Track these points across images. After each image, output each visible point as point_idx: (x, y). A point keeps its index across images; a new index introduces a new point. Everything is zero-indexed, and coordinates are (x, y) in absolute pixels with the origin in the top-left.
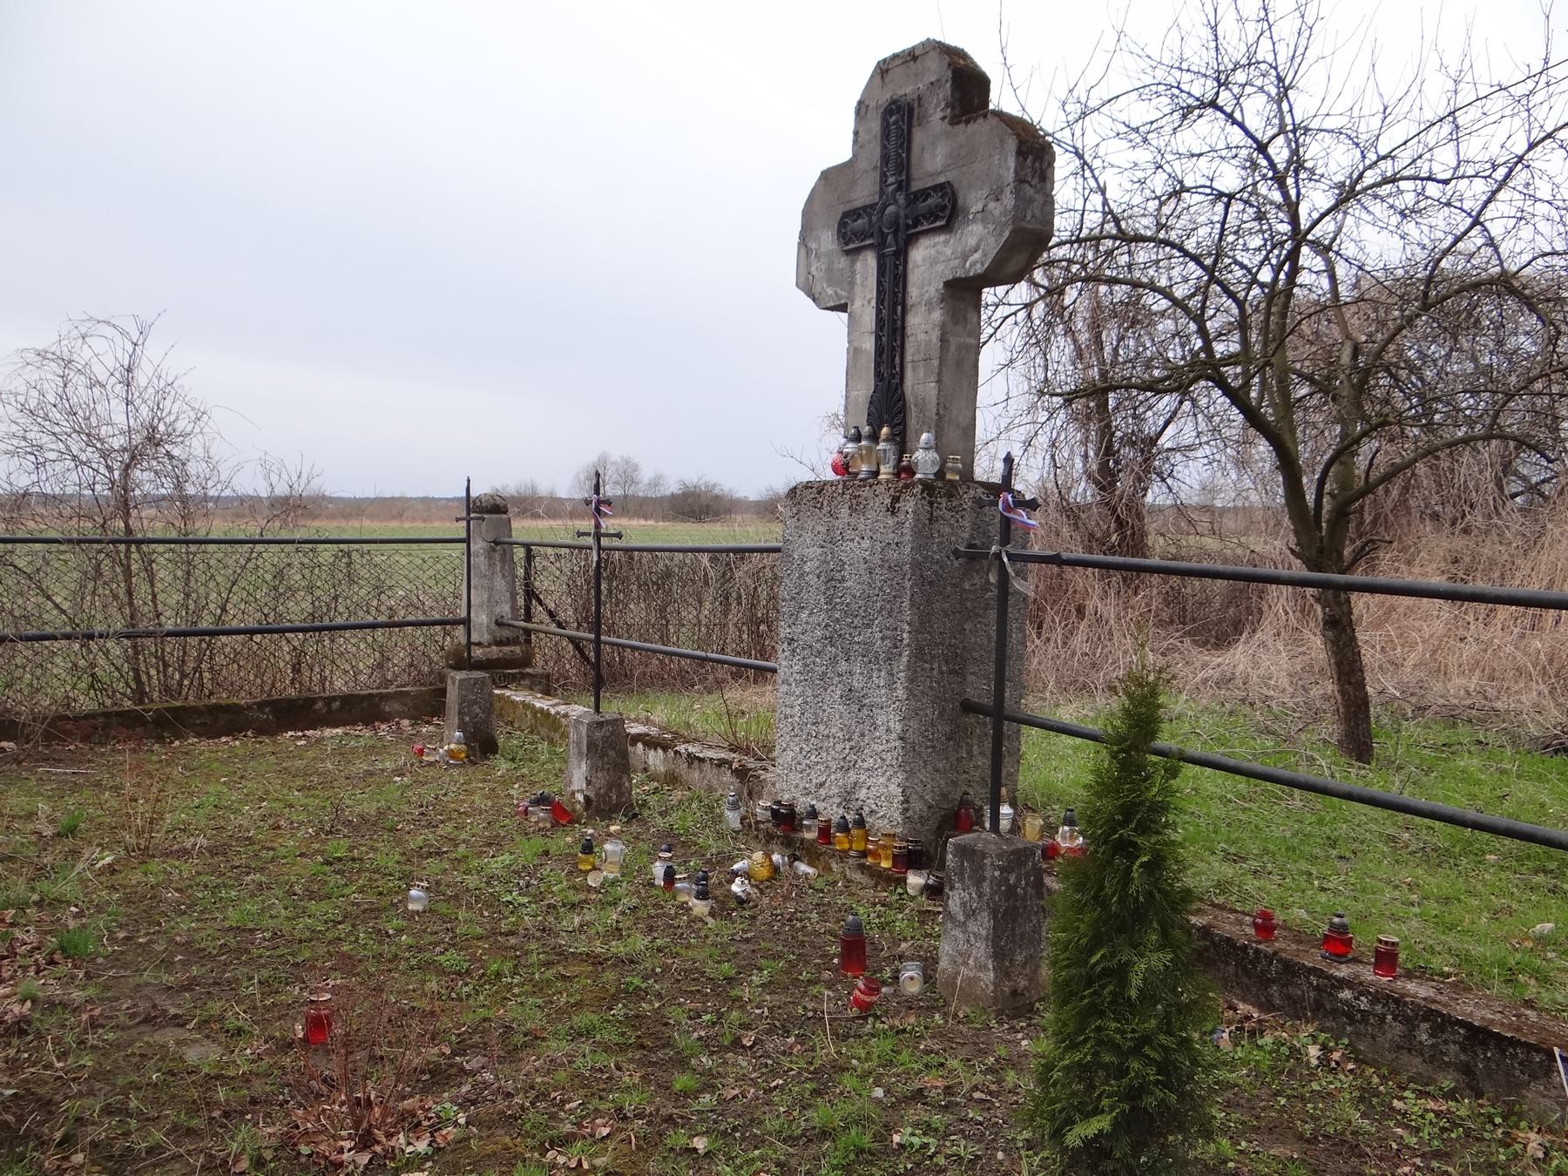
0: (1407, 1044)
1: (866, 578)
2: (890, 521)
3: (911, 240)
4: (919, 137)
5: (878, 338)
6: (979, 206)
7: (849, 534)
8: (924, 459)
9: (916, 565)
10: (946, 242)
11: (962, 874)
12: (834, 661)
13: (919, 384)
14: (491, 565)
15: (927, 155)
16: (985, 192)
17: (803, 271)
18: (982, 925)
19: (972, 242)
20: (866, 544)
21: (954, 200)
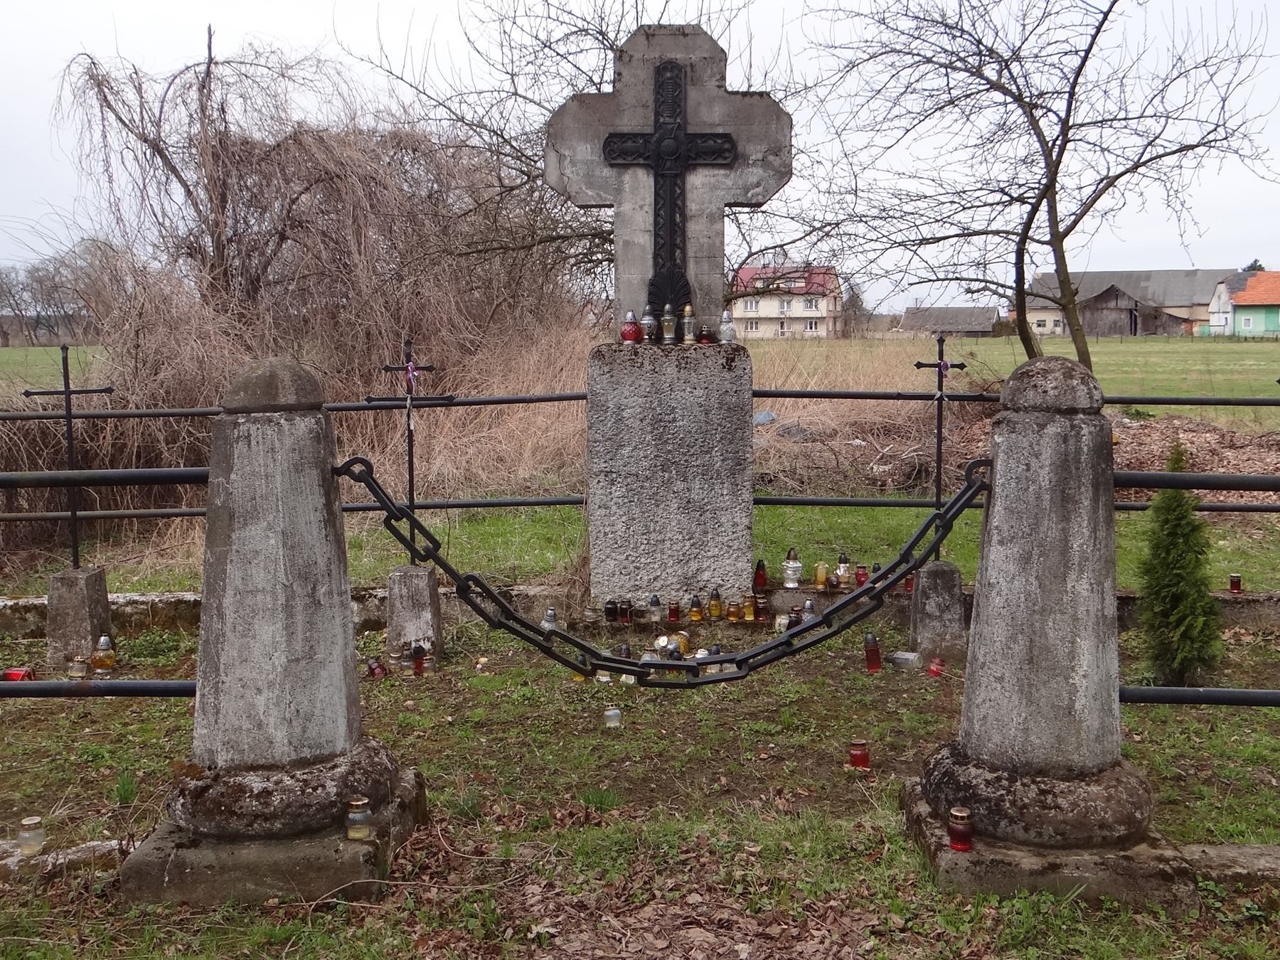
1: (703, 418)
2: (727, 375)
3: (694, 167)
6: (760, 156)
10: (727, 176)
11: (936, 588)
16: (764, 147)
19: (754, 180)
21: (734, 145)
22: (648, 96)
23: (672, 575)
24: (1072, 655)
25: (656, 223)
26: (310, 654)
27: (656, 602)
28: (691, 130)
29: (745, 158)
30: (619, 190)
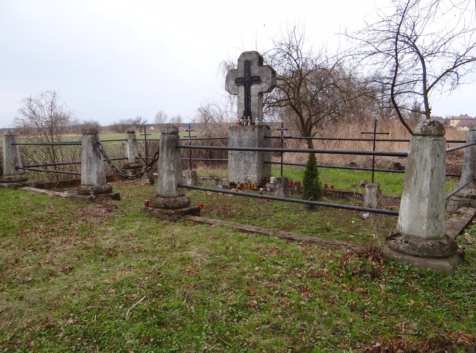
0: (336, 196)
2: (253, 132)
3: (251, 84)
4: (252, 67)
5: (245, 101)
7: (244, 135)
8: (257, 122)
9: (258, 139)
12: (242, 156)
13: (254, 109)
14: (134, 145)
15: (254, 71)
17: (246, 91)
18: (282, 188)
19: (264, 86)
20: (248, 136)
22: (243, 69)
23: (243, 177)
24: (163, 176)
25: (245, 98)
26: (90, 170)
27: (239, 183)
28: (252, 76)
29: (262, 81)
30: (238, 91)
